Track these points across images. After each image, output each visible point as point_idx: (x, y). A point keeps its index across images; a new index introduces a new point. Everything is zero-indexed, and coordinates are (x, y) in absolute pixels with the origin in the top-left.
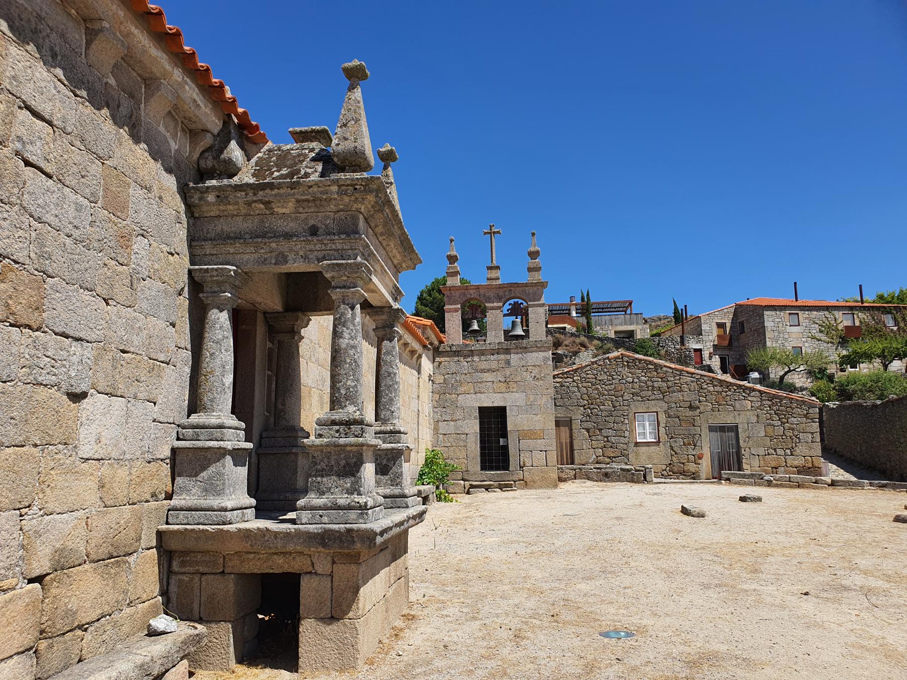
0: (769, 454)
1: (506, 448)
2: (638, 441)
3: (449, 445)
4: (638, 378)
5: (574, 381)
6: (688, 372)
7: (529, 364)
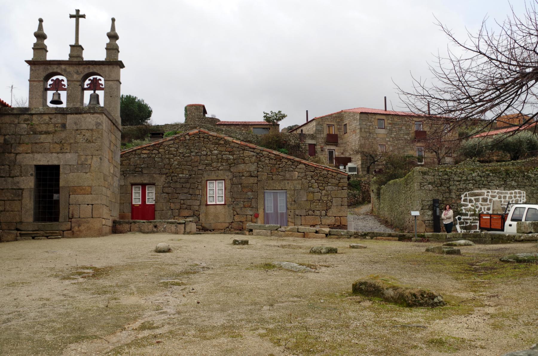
0: (309, 215)
1: (57, 202)
2: (209, 203)
3: (6, 199)
4: (211, 151)
5: (159, 153)
6: (250, 148)
7: (83, 128)
